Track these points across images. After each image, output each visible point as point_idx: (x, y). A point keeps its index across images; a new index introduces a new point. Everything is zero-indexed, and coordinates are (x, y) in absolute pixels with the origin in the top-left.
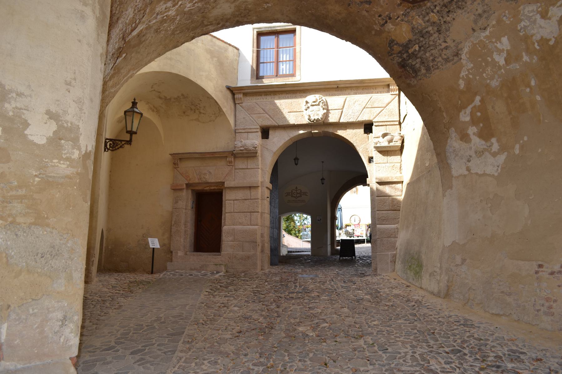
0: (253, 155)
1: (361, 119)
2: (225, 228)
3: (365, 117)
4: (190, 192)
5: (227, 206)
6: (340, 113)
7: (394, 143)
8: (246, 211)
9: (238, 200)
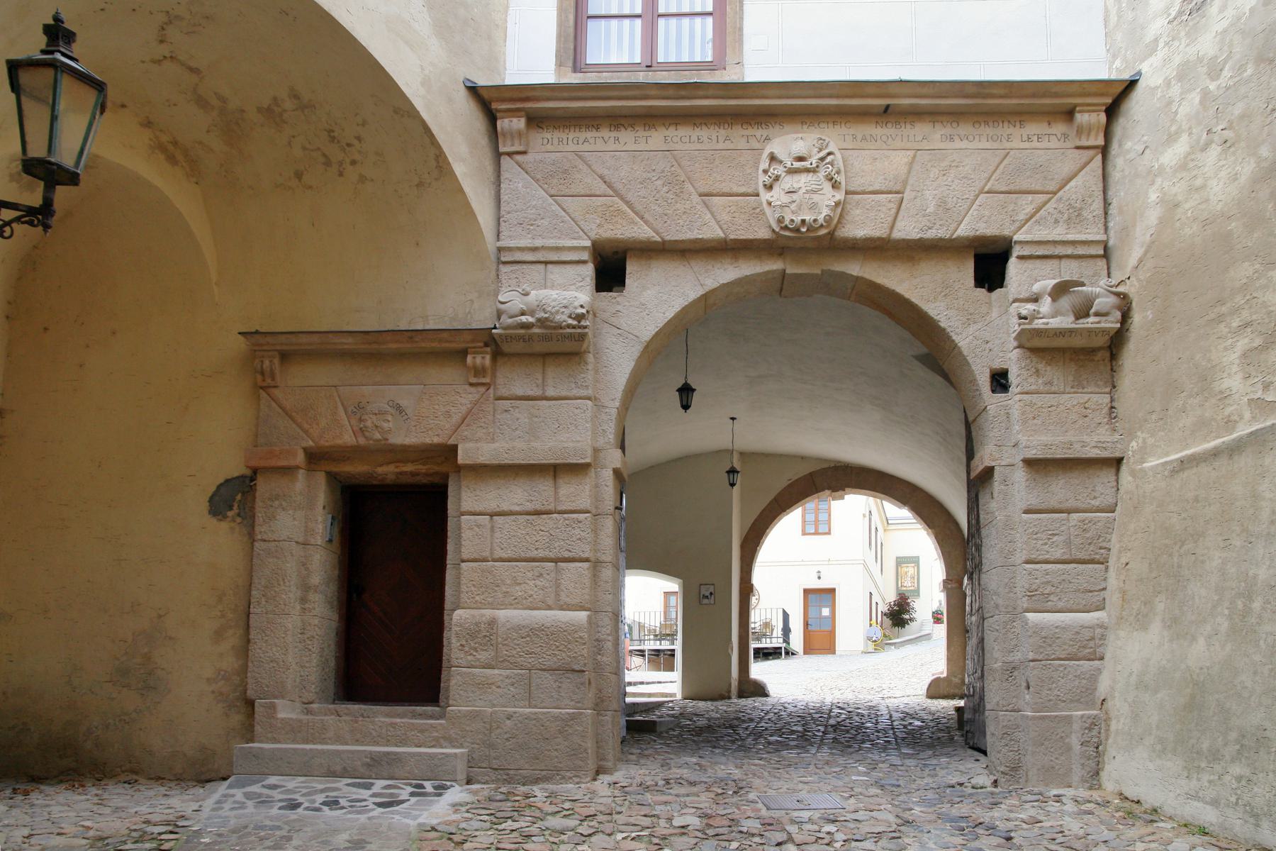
0: (568, 346)
1: (965, 230)
2: (459, 618)
3: (977, 222)
4: (321, 480)
5: (466, 534)
6: (894, 206)
7: (1092, 319)
8: (541, 554)
9: (511, 513)
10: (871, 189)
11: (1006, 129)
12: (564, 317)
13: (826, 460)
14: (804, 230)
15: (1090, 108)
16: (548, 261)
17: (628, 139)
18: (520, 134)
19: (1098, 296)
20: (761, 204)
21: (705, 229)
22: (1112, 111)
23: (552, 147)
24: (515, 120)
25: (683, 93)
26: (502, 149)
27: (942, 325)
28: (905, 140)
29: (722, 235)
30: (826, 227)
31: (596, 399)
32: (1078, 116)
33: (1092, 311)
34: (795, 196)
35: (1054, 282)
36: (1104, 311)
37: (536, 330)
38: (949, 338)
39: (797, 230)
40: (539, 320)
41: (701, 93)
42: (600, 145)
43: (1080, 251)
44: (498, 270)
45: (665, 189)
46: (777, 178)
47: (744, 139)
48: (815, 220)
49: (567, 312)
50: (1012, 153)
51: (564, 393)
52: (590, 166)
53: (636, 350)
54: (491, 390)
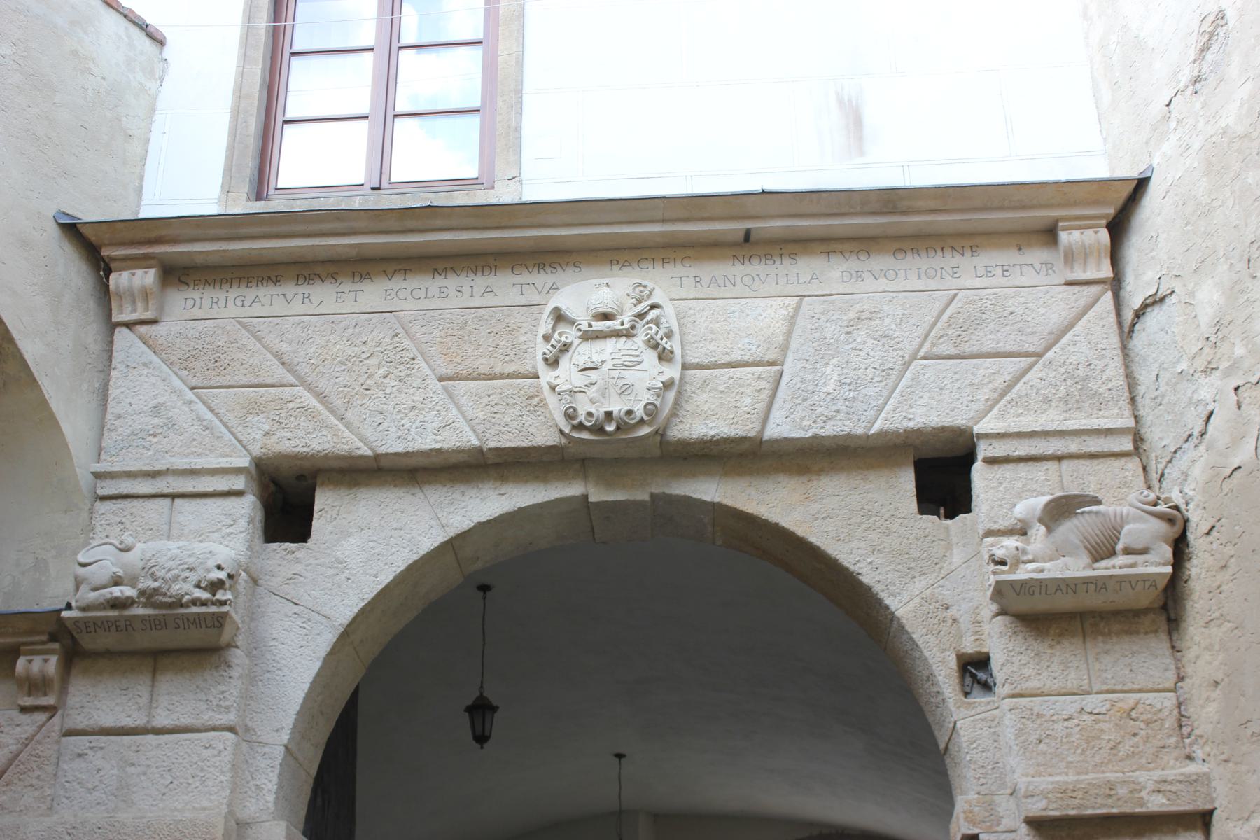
0: (195, 637)
3: (928, 407)
6: (767, 385)
7: (1121, 560)
10: (727, 359)
11: (950, 260)
12: (188, 587)
13: (811, 824)
14: (610, 428)
15: (1082, 223)
16: (175, 489)
17: (324, 297)
18: (146, 294)
19: (1123, 520)
20: (539, 391)
21: (446, 433)
22: (1118, 227)
23: (197, 315)
24: (139, 272)
25: (411, 224)
26: (116, 318)
27: (865, 580)
28: (782, 281)
29: (475, 442)
30: (650, 423)
31: (247, 729)
32: (1064, 236)
33: (1120, 547)
34: (594, 375)
35: (1047, 498)
36: (1139, 545)
37: (139, 611)
38: (880, 602)
39: (598, 429)
40: (142, 593)
41: (439, 222)
42: (279, 306)
43: (1094, 445)
44: (91, 511)
45: (382, 371)
46: (566, 348)
47: (517, 289)
48: (629, 413)
49: (194, 578)
50: (961, 294)
51: (185, 721)
52: (259, 340)
53: (325, 640)
54: (57, 719)
